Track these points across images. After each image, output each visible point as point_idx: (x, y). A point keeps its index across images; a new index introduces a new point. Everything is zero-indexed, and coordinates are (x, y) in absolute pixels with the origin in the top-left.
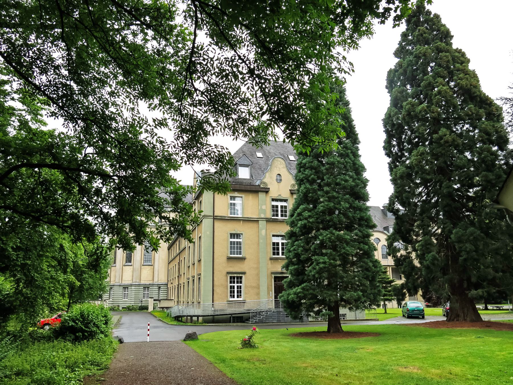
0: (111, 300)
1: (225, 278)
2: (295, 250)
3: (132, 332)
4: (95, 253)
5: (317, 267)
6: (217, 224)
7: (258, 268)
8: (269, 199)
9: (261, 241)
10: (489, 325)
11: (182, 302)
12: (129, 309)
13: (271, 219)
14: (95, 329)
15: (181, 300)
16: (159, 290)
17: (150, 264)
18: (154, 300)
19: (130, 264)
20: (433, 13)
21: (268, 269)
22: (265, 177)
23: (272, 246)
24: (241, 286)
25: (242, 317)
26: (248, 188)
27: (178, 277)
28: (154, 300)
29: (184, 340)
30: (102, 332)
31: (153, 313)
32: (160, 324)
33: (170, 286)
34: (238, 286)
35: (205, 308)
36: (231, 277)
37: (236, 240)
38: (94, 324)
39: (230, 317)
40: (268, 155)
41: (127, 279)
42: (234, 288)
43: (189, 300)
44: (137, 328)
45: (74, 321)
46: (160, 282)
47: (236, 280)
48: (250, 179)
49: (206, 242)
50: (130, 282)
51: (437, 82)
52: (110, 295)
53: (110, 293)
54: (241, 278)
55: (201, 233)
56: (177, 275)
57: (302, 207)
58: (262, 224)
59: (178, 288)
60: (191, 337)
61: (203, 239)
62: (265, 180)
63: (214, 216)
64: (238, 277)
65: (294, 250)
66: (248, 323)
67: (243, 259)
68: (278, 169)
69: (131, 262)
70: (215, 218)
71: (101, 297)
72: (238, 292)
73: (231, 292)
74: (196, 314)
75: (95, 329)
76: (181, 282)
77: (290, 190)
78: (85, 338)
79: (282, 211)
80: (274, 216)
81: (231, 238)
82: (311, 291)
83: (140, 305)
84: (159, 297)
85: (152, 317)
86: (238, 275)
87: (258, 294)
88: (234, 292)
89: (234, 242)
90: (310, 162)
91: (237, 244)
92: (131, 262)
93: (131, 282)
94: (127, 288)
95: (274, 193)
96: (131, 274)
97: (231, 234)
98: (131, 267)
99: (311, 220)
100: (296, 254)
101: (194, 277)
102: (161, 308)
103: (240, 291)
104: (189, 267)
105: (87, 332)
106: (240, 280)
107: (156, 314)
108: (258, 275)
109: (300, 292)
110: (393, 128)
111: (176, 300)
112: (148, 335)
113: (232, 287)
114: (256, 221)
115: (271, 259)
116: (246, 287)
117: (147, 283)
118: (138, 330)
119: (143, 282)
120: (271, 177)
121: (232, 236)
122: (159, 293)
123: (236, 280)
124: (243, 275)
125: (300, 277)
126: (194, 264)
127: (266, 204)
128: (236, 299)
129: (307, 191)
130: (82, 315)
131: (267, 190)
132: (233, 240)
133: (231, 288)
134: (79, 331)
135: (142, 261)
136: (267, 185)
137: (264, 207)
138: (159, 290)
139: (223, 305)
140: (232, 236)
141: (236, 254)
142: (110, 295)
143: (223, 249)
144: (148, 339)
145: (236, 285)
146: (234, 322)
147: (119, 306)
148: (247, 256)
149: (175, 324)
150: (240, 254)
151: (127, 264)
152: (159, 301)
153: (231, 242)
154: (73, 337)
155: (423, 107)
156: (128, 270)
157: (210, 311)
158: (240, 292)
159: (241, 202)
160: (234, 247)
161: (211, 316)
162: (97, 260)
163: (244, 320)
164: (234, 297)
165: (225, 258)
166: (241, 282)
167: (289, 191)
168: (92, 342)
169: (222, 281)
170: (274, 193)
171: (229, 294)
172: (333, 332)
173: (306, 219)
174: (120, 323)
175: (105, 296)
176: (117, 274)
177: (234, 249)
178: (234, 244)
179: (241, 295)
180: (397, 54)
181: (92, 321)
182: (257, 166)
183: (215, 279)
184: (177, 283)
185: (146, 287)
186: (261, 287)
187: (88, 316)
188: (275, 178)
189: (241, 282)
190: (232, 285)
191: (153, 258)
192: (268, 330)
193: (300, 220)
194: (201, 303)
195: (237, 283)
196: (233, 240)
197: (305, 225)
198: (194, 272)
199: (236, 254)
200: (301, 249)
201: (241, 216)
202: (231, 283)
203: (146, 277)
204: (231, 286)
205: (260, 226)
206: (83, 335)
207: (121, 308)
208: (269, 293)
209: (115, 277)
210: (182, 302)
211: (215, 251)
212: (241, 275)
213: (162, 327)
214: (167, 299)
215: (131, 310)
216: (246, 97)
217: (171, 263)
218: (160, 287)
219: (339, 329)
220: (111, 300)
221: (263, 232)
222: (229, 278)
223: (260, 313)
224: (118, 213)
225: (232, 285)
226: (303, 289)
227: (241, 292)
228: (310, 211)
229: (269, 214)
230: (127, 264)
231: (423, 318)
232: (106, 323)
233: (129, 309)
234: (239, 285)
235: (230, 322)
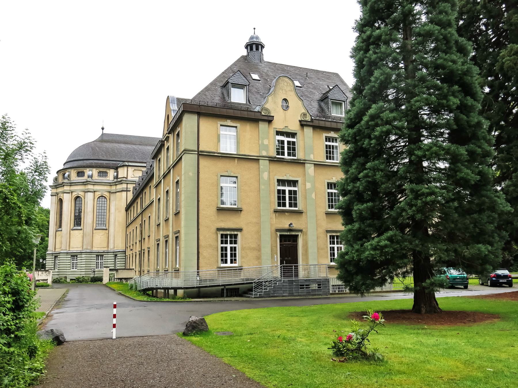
0: (56, 270)
1: (215, 236)
2: (369, 177)
6: (203, 162)
7: (258, 224)
8: (272, 132)
9: (262, 187)
11: (146, 272)
12: (79, 281)
13: (275, 157)
15: (145, 268)
16: (115, 259)
17: (105, 228)
19: (79, 228)
21: (271, 225)
22: (267, 102)
23: (276, 195)
24: (235, 248)
25: (238, 289)
26: (245, 115)
27: (140, 241)
28: (110, 270)
29: (184, 334)
31: (109, 286)
32: (122, 300)
33: (128, 253)
34: (231, 248)
35: (187, 277)
36: (222, 236)
39: (223, 290)
40: (266, 78)
41: (76, 246)
42: (226, 250)
43: (160, 268)
44: (90, 307)
47: (229, 239)
48: (246, 104)
49: (187, 189)
50: (79, 250)
52: (54, 265)
54: (236, 236)
55: (169, 186)
56: (139, 238)
58: (264, 164)
59: (140, 255)
60: (196, 328)
61: (182, 184)
62: (267, 106)
63: (198, 151)
64: (231, 236)
65: (367, 176)
66: (249, 297)
68: (284, 92)
69: (80, 226)
70: (201, 154)
72: (231, 256)
73: (222, 256)
74: (174, 285)
76: (145, 247)
77: (300, 121)
79: (289, 149)
80: (278, 154)
83: (92, 276)
84: (115, 266)
85: (107, 288)
86: (232, 233)
87: (259, 258)
88: (226, 256)
92: (80, 226)
93: (81, 249)
94: (76, 256)
95: (278, 124)
96: (81, 239)
98: (81, 232)
100: (369, 182)
102: (119, 279)
103: (235, 254)
104: (159, 225)
106: (234, 239)
107: (114, 286)
108: (259, 232)
111: (138, 269)
112: (114, 326)
113: (224, 249)
114: (256, 160)
115: (276, 211)
116: (243, 249)
117: (101, 250)
118: (93, 311)
119: (95, 249)
120: (275, 102)
122: (115, 262)
123: (229, 239)
124: (239, 233)
126: (167, 220)
127: (268, 138)
128: (229, 264)
131: (270, 119)
133: (222, 250)
135: (95, 225)
136: (269, 112)
137: (266, 142)
138: (115, 259)
139: (211, 271)
142: (54, 265)
145: (229, 246)
147: (66, 277)
148: (244, 208)
149: (145, 299)
151: (75, 228)
152: (117, 270)
156: (77, 235)
158: (234, 255)
159: (235, 134)
161: (197, 287)
163: (240, 292)
165: (215, 209)
166: (235, 243)
167: (298, 123)
169: (211, 242)
170: (278, 124)
172: (427, 312)
174: (66, 299)
176: (64, 240)
179: (235, 260)
182: (254, 90)
183: (201, 238)
184: (138, 249)
185: (100, 255)
186: (262, 249)
188: (281, 104)
189: (235, 243)
190: (224, 245)
191: (107, 221)
192: (304, 308)
194: (182, 270)
195: (231, 243)
198: (168, 230)
201: (235, 153)
202: (222, 243)
203: (99, 243)
204: (222, 248)
207: (68, 280)
208: (272, 257)
209: (61, 243)
210: (146, 272)
211: (200, 199)
212: (236, 233)
213: (128, 305)
214: (125, 269)
215: (81, 282)
217: (130, 227)
218: (116, 255)
219: (435, 307)
220: (56, 270)
221: (265, 175)
222: (219, 236)
223: (259, 284)
225: (224, 245)
226: (390, 239)
227: (235, 256)
229: (273, 153)
230: (75, 228)
231: (466, 287)
233: (79, 281)
234: (233, 245)
235: (222, 296)
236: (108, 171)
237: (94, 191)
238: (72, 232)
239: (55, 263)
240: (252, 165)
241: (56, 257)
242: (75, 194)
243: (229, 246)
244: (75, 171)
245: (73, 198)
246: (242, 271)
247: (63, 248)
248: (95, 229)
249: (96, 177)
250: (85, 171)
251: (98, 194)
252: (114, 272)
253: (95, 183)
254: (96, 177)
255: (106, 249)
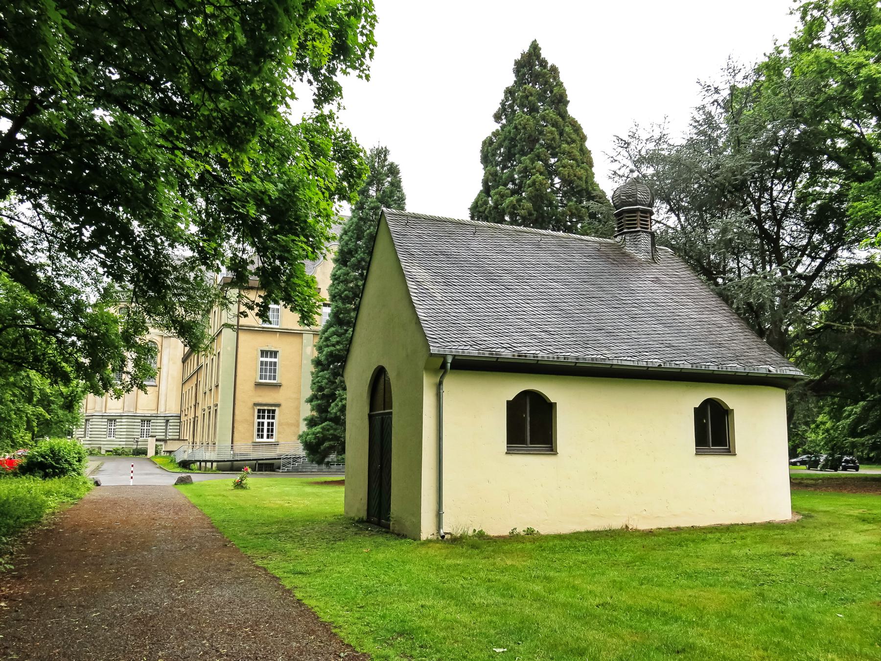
0: (87, 438)
3: (114, 478)
4: (70, 396)
5: (340, 404)
6: (243, 336)
12: (117, 453)
14: (66, 466)
17: (153, 384)
18: (157, 440)
20: (549, 65)
24: (273, 423)
25: (273, 464)
27: (195, 406)
28: (157, 440)
30: (74, 470)
31: (154, 460)
32: (159, 471)
33: (183, 418)
34: (268, 423)
36: (259, 411)
37: (269, 360)
38: (66, 460)
42: (263, 425)
45: (43, 457)
46: (168, 413)
49: (226, 361)
50: (119, 412)
51: (535, 168)
52: (85, 431)
53: (85, 428)
54: (274, 411)
56: (193, 403)
57: (332, 329)
59: (194, 422)
64: (269, 411)
67: (278, 386)
71: (70, 433)
72: (268, 431)
73: (258, 431)
75: (66, 466)
78: (55, 474)
82: (331, 432)
83: (135, 447)
84: (166, 435)
85: (151, 463)
88: (263, 431)
89: (266, 362)
90: (345, 274)
91: (271, 365)
97: (262, 352)
99: (338, 347)
101: (210, 408)
105: (57, 468)
106: (272, 414)
109: (318, 432)
111: (191, 440)
113: (261, 424)
116: (280, 424)
119: (140, 412)
122: (166, 429)
124: (277, 409)
125: (324, 415)
126: (211, 390)
128: (265, 439)
129: (338, 311)
130: (52, 451)
132: (264, 359)
133: (259, 425)
134: (49, 467)
139: (246, 446)
140: (264, 353)
141: (268, 378)
142: (85, 431)
143: (250, 371)
144: (131, 483)
145: (266, 421)
146: (259, 470)
147: (100, 448)
148: (284, 383)
150: (275, 379)
153: (262, 362)
154: (42, 473)
155: (512, 201)
157: (227, 455)
158: (271, 431)
160: (266, 369)
162: (71, 401)
164: (262, 437)
165: (253, 384)
166: (273, 418)
168: (63, 479)
169: (247, 415)
171: (256, 433)
173: (334, 345)
175: (78, 432)
177: (266, 372)
178: (266, 365)
180: (497, 117)
181: (63, 457)
183: (237, 412)
185: (146, 420)
187: (59, 452)
190: (261, 420)
193: (328, 346)
195: (268, 418)
196: (264, 359)
197: (331, 352)
199: (268, 378)
200: (325, 381)
205: (305, 341)
206: (54, 472)
207: (103, 452)
214: (179, 440)
215: (119, 455)
217: (187, 384)
218: (167, 421)
220: (87, 438)
222: (256, 411)
224: (92, 362)
225: (261, 420)
226: (323, 428)
227: (272, 431)
228: (339, 335)
232: (79, 461)
233: (117, 453)
234: (271, 421)
240: (294, 340)
246: (278, 447)
247: (98, 409)
252: (162, 443)
255: (155, 412)
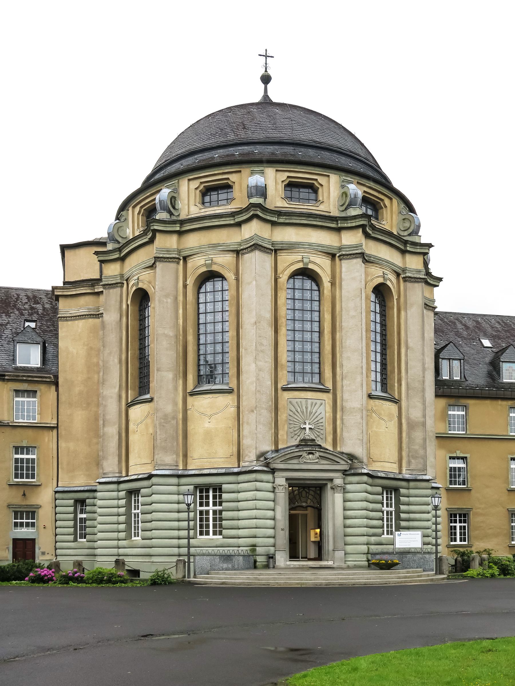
10: (233, 214)
34: (460, 527)
47: (458, 519)
52: (128, 523)
72: (461, 535)
81: (16, 453)
110: (394, 308)
121: (18, 449)
123: (458, 519)
128: (458, 542)
145: (458, 525)
156: (211, 414)
190: (204, 508)
195: (460, 522)
202: (201, 505)
216: (216, 376)
225: (204, 508)
236: (322, 180)
237: (276, 251)
238: (190, 399)
239: (128, 514)
241: (133, 493)
242: (198, 264)
243: (458, 525)
244: (195, 184)
245: (190, 281)
248: (285, 389)
249: (276, 199)
250: (233, 178)
251: (290, 262)
253: (277, 218)
254: (276, 199)
